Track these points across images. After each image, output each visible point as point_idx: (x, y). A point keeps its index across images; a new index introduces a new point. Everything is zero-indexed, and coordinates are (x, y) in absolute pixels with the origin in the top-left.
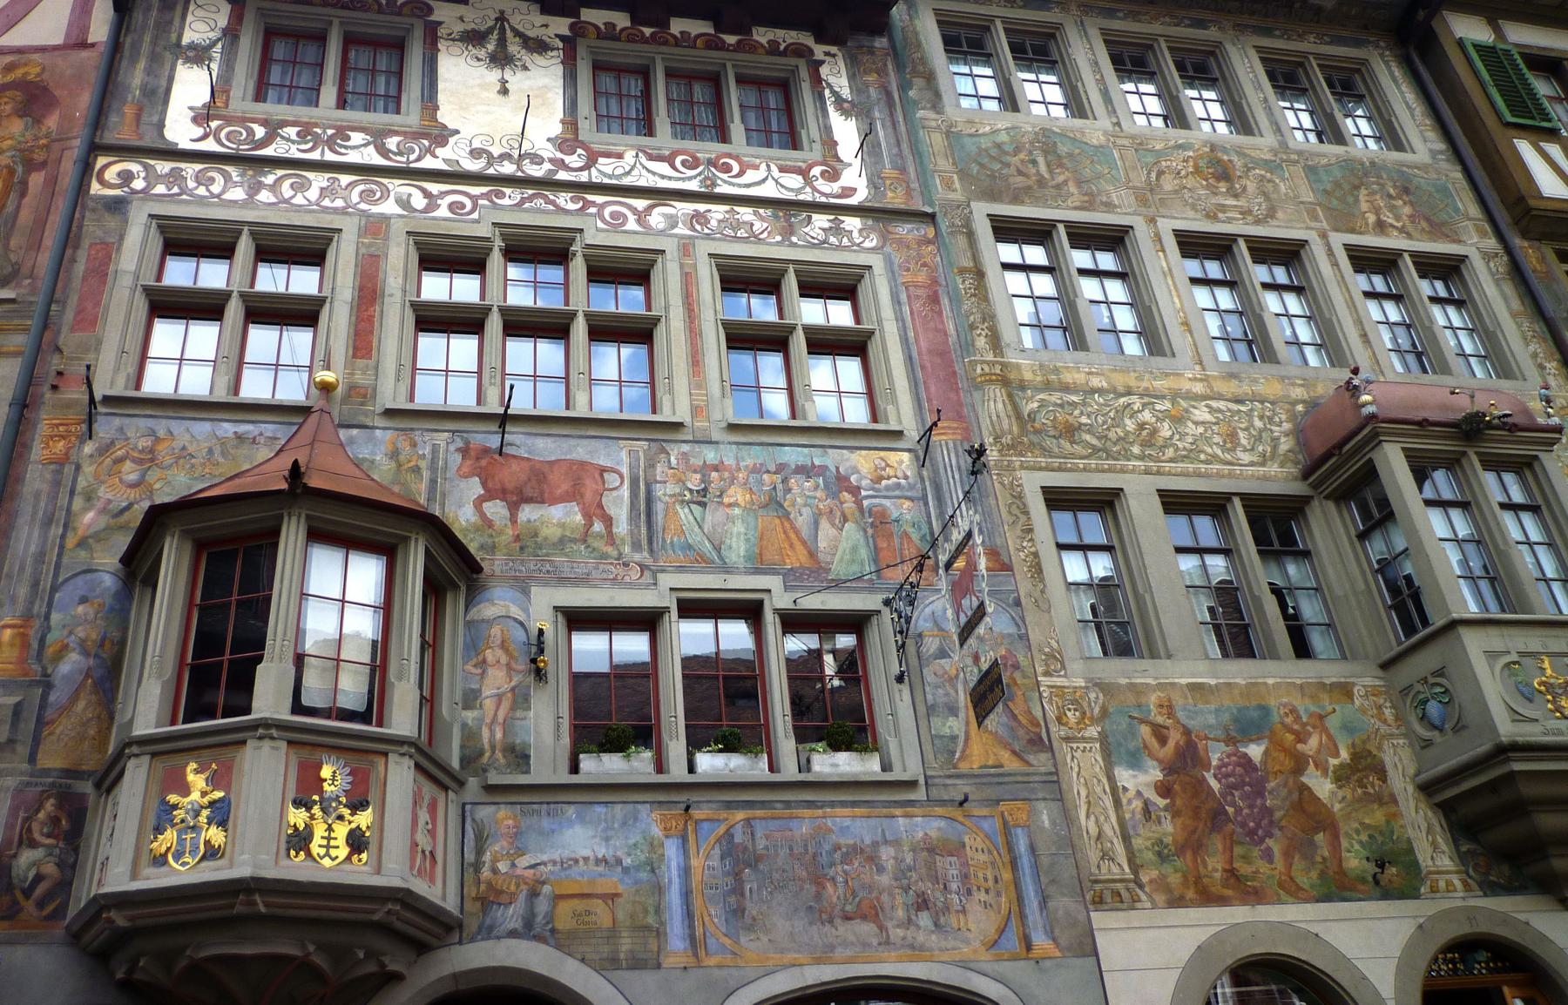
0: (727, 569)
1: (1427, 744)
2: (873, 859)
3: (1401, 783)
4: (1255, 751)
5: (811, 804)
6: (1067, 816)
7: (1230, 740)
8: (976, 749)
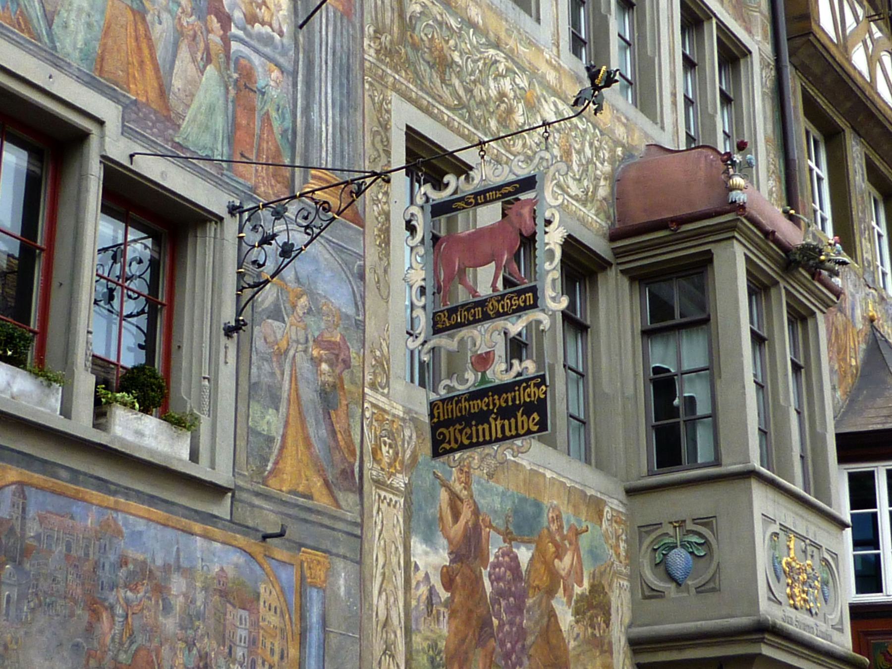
0: (56, 61)
1: (655, 594)
2: (160, 590)
3: (618, 636)
4: (524, 554)
5: (102, 485)
6: (362, 583)
7: (508, 537)
8: (289, 465)
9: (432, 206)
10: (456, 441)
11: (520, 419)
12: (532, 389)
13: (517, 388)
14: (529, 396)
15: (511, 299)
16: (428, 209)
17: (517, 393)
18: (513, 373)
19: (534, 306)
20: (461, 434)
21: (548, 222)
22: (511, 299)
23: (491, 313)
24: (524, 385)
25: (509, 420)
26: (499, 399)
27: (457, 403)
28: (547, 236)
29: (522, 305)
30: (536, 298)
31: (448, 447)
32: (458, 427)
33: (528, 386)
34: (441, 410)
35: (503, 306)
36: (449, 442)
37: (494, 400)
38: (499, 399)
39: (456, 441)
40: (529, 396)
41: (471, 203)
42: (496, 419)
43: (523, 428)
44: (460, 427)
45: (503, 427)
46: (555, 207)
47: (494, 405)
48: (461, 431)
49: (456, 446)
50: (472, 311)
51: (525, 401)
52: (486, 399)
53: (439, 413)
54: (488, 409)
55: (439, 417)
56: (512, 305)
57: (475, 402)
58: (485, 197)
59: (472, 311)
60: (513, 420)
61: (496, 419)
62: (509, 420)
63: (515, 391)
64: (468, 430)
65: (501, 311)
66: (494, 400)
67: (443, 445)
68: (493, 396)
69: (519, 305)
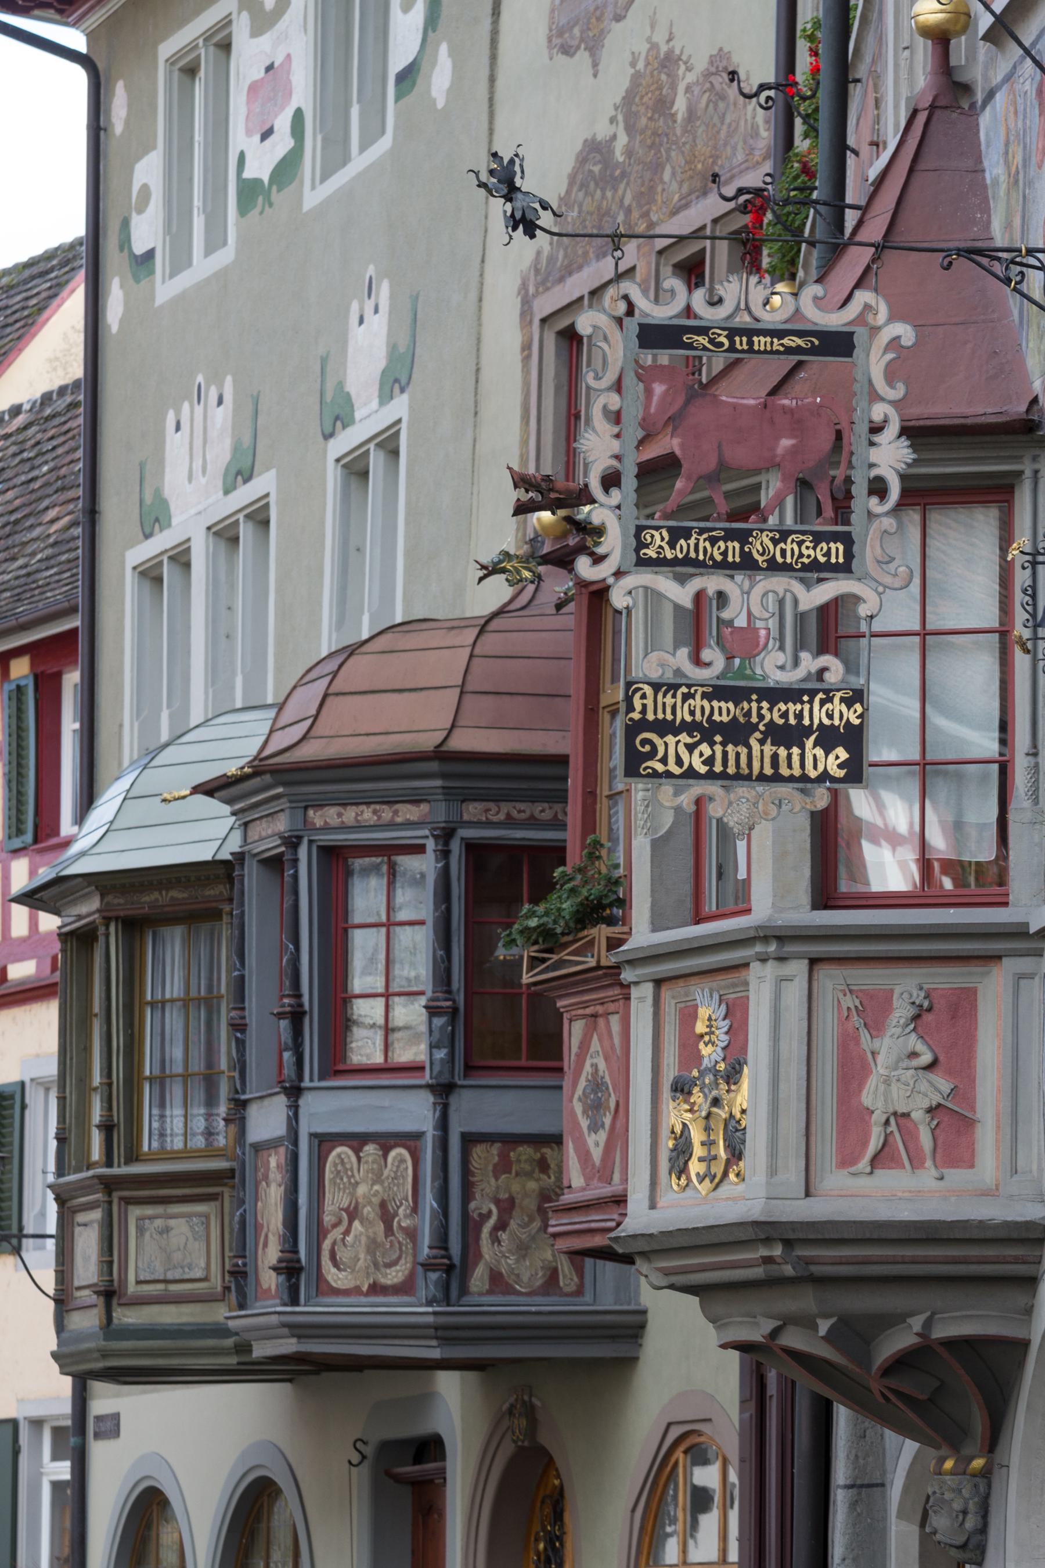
9: (641, 326)
10: (679, 762)
11: (756, 746)
12: (837, 706)
13: (806, 698)
14: (830, 716)
15: (800, 544)
16: (632, 326)
17: (807, 707)
18: (800, 673)
19: (845, 568)
20: (691, 753)
21: (876, 429)
22: (800, 544)
23: (760, 559)
24: (684, 690)
25: (788, 748)
26: (770, 710)
27: (686, 697)
28: (873, 450)
29: (822, 560)
30: (849, 555)
31: (660, 767)
32: (684, 738)
33: (830, 700)
34: (649, 702)
35: (783, 552)
36: (664, 761)
37: (760, 708)
38: (770, 710)
39: (679, 762)
40: (830, 716)
41: (722, 344)
42: (762, 742)
43: (815, 767)
44: (689, 740)
45: (775, 757)
46: (890, 402)
47: (761, 717)
48: (690, 748)
49: (677, 770)
50: (721, 544)
51: (683, 720)
52: (746, 705)
53: (644, 706)
54: (694, 720)
55: (644, 711)
56: (801, 555)
57: (723, 704)
58: (750, 343)
59: (721, 544)
60: (795, 751)
61: (762, 742)
62: (788, 748)
63: (750, 701)
64: (705, 748)
65: (780, 560)
66: (760, 708)
67: (649, 764)
68: (759, 701)
69: (647, 546)
